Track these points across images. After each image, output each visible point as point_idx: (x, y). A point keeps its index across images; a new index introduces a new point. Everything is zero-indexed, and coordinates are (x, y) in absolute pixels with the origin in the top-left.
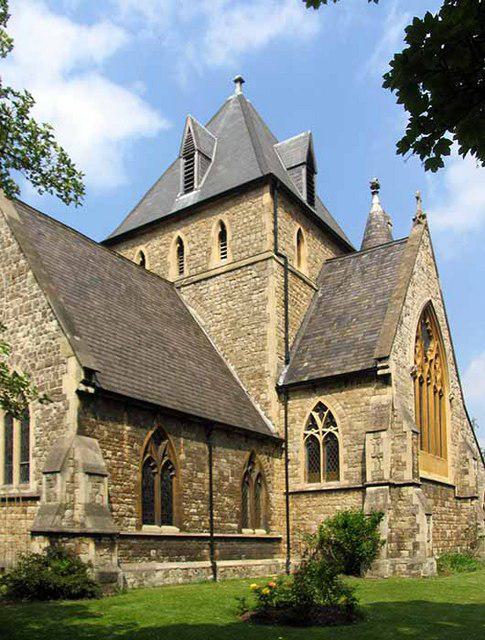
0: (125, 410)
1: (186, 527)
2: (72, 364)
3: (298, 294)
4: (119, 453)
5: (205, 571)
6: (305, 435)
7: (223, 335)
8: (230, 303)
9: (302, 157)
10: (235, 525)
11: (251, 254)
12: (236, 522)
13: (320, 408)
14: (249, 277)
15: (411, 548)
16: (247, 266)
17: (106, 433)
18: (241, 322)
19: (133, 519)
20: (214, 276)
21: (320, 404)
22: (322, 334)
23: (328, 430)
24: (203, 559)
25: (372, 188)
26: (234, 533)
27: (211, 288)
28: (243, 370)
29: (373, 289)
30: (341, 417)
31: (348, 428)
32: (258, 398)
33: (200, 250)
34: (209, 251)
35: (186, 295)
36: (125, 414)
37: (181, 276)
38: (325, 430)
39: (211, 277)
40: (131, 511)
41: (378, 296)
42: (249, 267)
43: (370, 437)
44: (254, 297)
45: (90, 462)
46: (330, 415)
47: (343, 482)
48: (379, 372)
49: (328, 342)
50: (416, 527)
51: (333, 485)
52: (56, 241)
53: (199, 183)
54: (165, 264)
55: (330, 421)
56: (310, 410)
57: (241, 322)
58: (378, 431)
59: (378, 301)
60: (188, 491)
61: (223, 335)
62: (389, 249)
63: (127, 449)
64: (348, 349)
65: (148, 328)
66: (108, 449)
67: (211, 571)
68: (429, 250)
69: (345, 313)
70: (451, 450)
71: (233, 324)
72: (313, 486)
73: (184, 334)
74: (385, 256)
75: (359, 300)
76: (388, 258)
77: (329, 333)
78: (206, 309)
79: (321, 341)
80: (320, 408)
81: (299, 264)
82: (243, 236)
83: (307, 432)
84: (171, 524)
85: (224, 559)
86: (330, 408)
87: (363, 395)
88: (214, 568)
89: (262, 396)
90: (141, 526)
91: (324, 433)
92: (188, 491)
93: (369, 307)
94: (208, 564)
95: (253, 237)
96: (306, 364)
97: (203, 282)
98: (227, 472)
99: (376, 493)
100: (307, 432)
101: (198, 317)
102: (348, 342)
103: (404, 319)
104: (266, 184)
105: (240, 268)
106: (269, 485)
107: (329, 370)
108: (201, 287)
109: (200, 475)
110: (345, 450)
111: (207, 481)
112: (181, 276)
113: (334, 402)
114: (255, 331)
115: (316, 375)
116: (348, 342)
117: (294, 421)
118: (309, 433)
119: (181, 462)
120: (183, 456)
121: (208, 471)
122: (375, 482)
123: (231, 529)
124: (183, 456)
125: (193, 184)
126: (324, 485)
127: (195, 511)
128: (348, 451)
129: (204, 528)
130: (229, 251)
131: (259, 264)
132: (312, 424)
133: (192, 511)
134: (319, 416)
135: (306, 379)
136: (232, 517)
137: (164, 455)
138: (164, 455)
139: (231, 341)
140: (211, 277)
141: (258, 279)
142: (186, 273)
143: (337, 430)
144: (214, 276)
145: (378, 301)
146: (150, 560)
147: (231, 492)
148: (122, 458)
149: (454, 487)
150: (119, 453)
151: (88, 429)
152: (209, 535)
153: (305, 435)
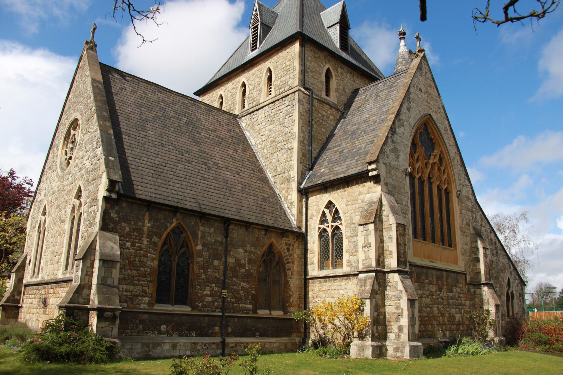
0: (148, 211)
1: (198, 306)
2: (105, 176)
3: (323, 116)
4: (137, 245)
5: (214, 346)
6: (319, 228)
7: (265, 150)
8: (271, 126)
9: (337, 18)
10: (250, 306)
11: (286, 89)
12: (250, 303)
13: (330, 205)
14: (283, 106)
15: (396, 331)
16: (282, 98)
17: (127, 229)
18: (277, 140)
19: (147, 299)
20: (262, 107)
21: (330, 203)
22: (339, 145)
23: (335, 224)
24: (213, 335)
25: (400, 34)
26: (247, 313)
27: (260, 117)
28: (277, 176)
29: (381, 108)
30: (345, 213)
31: (349, 222)
32: (286, 198)
33: (255, 90)
34: (260, 91)
35: (244, 123)
36: (147, 214)
37: (243, 110)
38: (333, 224)
39: (260, 109)
40: (144, 291)
41: (383, 114)
42: (284, 99)
43: (361, 228)
44: (286, 121)
45: (107, 251)
46: (337, 211)
47: (345, 269)
48: (371, 174)
49: (341, 152)
50: (400, 311)
51: (338, 271)
52: (136, 92)
53: (260, 44)
54: (234, 103)
55: (336, 216)
56: (322, 208)
57: (277, 140)
58: (367, 224)
59: (382, 117)
60: (203, 276)
61: (265, 150)
62: (398, 77)
63: (145, 242)
64: (353, 157)
65: (195, 149)
66: (128, 241)
67: (220, 346)
68: (429, 75)
69: (358, 129)
70: (460, 239)
71: (273, 142)
72: (323, 273)
73: (231, 152)
74: (394, 83)
75: (370, 117)
76: (395, 84)
77: (344, 145)
78: (256, 132)
79: (336, 152)
80: (330, 205)
81: (328, 94)
82: (282, 77)
83: (320, 226)
84: (186, 305)
85: (235, 336)
86: (337, 206)
87: (360, 193)
88: (223, 343)
89: (289, 197)
90: (153, 305)
91: (332, 226)
92: (203, 276)
93: (375, 122)
94: (218, 340)
95: (288, 77)
96: (323, 170)
97: (255, 112)
98: (244, 260)
99: (365, 279)
100: (320, 226)
101: (251, 138)
102: (354, 151)
103: (397, 130)
104: (296, 40)
105: (278, 100)
106: (288, 272)
107: (337, 174)
108: (254, 117)
109: (216, 263)
110: (347, 240)
111: (222, 268)
112: (243, 110)
113: (336, 197)
114: (286, 146)
115: (327, 178)
116: (354, 151)
117: (312, 217)
118: (322, 227)
119: (197, 251)
120: (199, 247)
121: (223, 259)
122: (365, 270)
123: (246, 310)
124: (199, 247)
125: (256, 45)
126: (330, 271)
127: (209, 293)
128: (349, 242)
129: (217, 308)
130: (273, 90)
131: (290, 96)
132: (323, 220)
133: (205, 292)
134: (330, 212)
135: (320, 182)
136: (247, 299)
137: (182, 246)
138: (182, 246)
139: (270, 155)
140: (260, 109)
141: (289, 107)
142: (247, 107)
143: (341, 224)
144: (262, 107)
145: (382, 117)
146: (160, 332)
147: (247, 277)
148: (141, 249)
149: (465, 274)
150: (137, 245)
151: (111, 226)
152: (221, 314)
153: (319, 228)
